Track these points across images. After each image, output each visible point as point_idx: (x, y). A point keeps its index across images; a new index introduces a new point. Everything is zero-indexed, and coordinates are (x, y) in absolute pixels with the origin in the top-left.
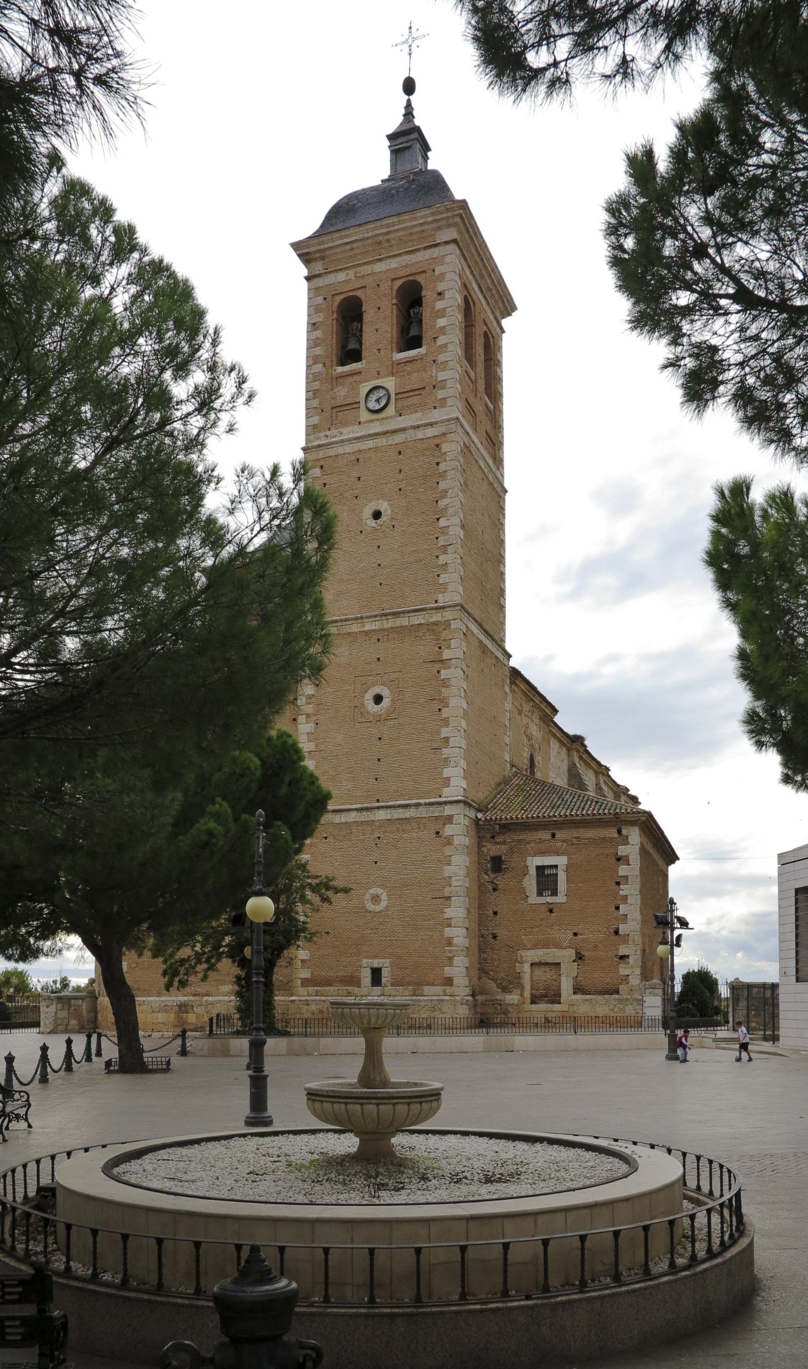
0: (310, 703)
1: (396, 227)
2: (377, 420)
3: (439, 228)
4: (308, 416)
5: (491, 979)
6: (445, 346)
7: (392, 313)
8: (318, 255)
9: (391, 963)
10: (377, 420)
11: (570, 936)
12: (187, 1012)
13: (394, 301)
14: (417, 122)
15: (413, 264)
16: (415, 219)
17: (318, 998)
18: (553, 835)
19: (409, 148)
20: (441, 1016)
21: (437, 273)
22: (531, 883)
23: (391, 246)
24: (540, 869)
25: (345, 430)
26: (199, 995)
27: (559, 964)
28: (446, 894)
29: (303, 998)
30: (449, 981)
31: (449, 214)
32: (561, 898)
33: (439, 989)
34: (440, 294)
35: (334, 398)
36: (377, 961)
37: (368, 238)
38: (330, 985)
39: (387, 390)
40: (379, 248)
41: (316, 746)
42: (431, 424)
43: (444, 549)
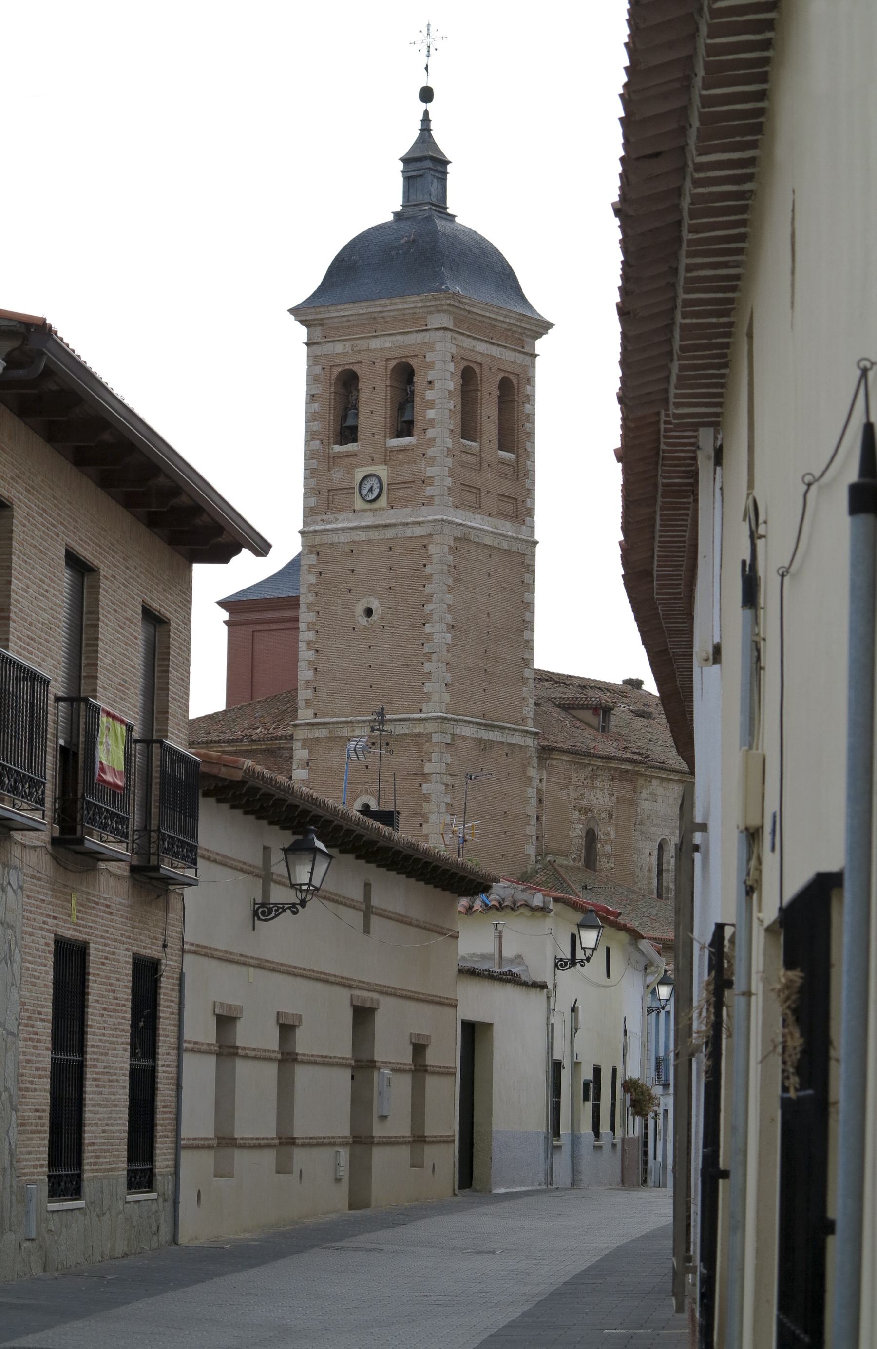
1: (389, 308)
3: (430, 313)
7: (386, 395)
10: (371, 510)
14: (470, 204)
15: (405, 347)
16: (406, 303)
21: (428, 360)
34: (430, 383)
35: (331, 480)
42: (419, 523)
43: (428, 657)
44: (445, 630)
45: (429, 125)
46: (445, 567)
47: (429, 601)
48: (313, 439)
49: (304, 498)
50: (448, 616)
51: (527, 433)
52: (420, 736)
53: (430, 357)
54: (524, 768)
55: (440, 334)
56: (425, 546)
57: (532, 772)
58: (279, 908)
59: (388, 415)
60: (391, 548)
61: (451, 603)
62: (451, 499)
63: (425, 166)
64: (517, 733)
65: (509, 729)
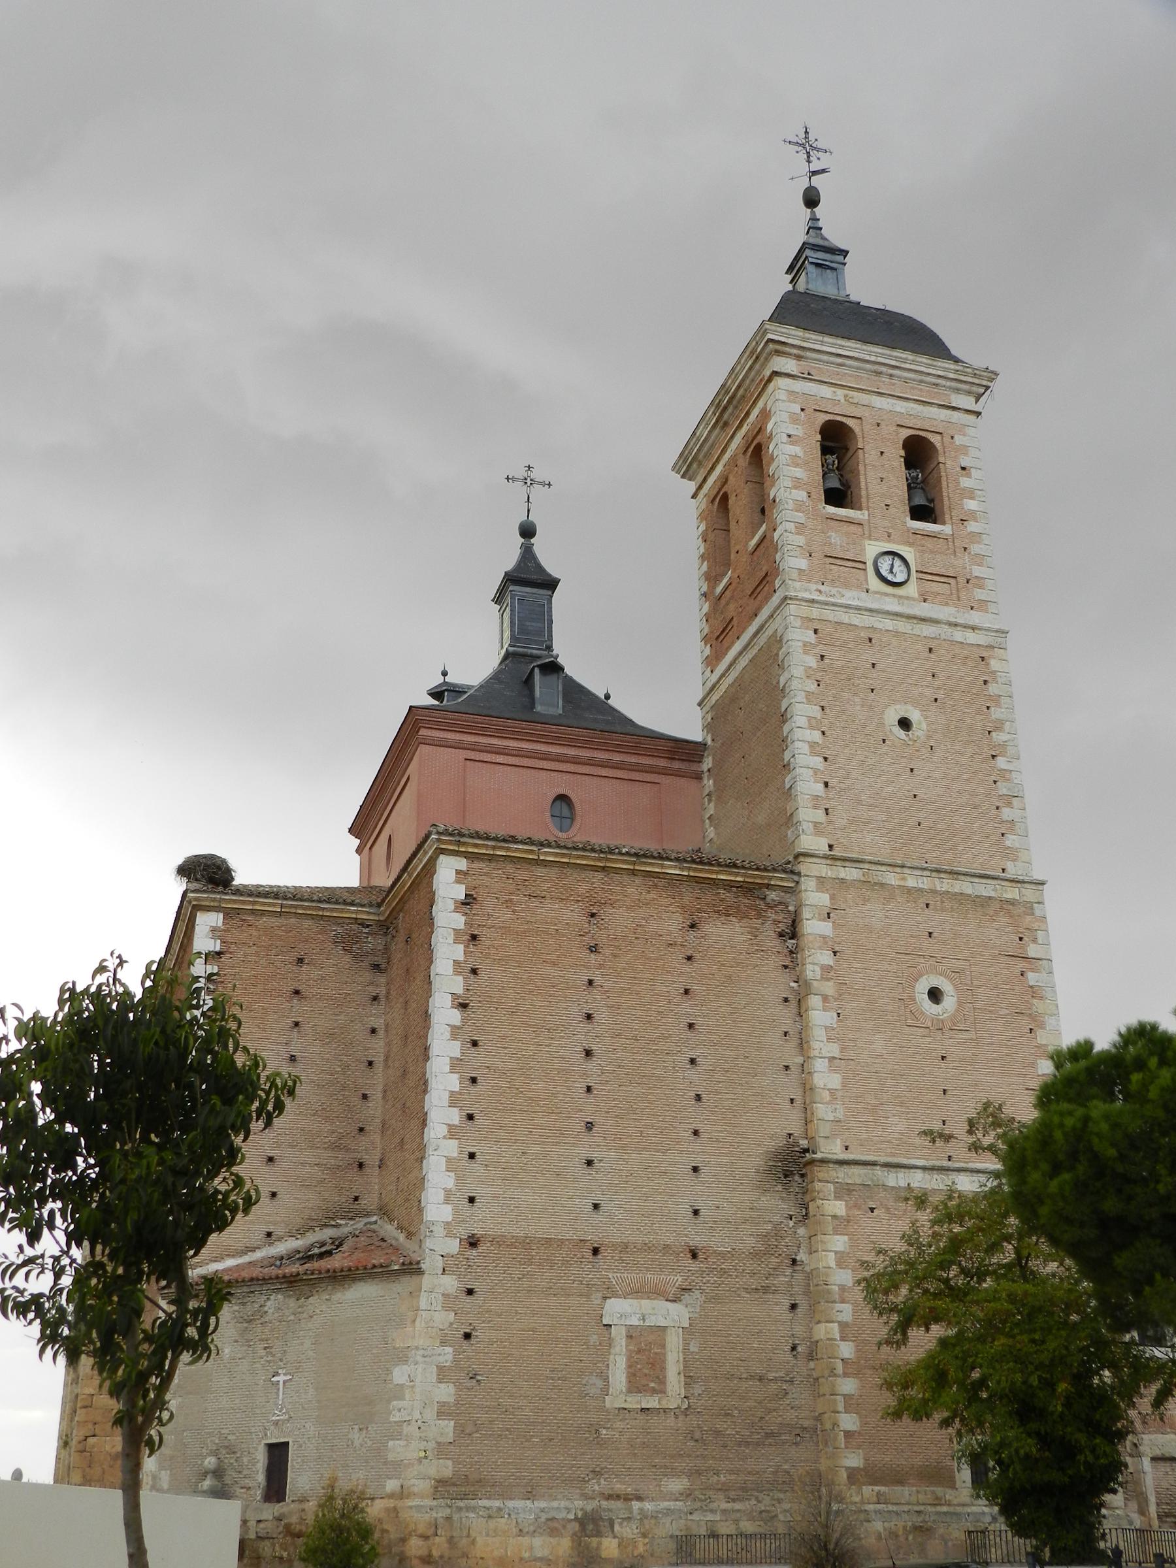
0: (828, 980)
1: (907, 366)
2: (894, 595)
10: (894, 595)
12: (599, 1534)
26: (618, 1497)
34: (963, 469)
37: (868, 362)
38: (901, 1482)
41: (842, 1050)
52: (1013, 904)
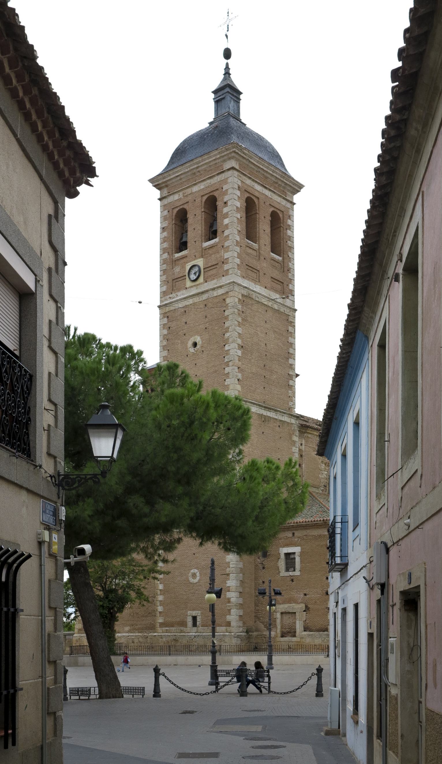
1: (201, 164)
3: (225, 161)
4: (161, 286)
5: (261, 622)
6: (228, 236)
7: (202, 217)
8: (164, 185)
9: (202, 613)
10: (195, 286)
11: (302, 596)
13: (203, 210)
15: (211, 186)
16: (211, 157)
17: (167, 634)
18: (293, 534)
19: (224, 98)
20: (224, 644)
21: (224, 190)
22: (282, 564)
23: (201, 174)
24: (287, 555)
25: (179, 294)
27: (295, 613)
28: (227, 572)
29: (160, 634)
30: (229, 624)
31: (228, 152)
32: (297, 573)
33: (223, 629)
34: (225, 203)
35: (174, 274)
36: (194, 612)
37: (188, 172)
38: (173, 626)
39: (199, 267)
40: (195, 177)
42: (221, 287)
44: (237, 348)
45: (229, 71)
46: (236, 311)
47: (227, 332)
48: (164, 253)
49: (161, 287)
50: (238, 339)
51: (289, 246)
53: (225, 187)
54: (290, 436)
55: (230, 172)
56: (224, 300)
57: (295, 438)
58: (82, 478)
59: (203, 229)
60: (206, 305)
61: (240, 332)
62: (239, 271)
63: (227, 94)
64: (285, 415)
65: (280, 412)
